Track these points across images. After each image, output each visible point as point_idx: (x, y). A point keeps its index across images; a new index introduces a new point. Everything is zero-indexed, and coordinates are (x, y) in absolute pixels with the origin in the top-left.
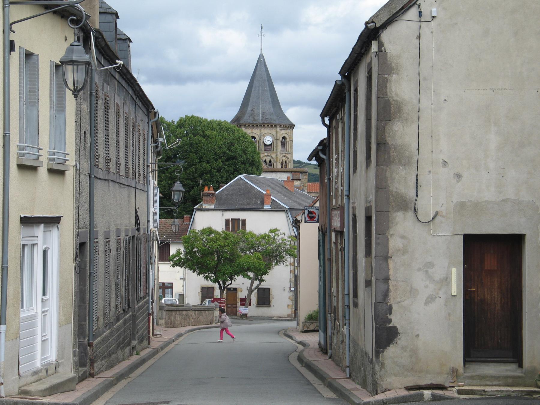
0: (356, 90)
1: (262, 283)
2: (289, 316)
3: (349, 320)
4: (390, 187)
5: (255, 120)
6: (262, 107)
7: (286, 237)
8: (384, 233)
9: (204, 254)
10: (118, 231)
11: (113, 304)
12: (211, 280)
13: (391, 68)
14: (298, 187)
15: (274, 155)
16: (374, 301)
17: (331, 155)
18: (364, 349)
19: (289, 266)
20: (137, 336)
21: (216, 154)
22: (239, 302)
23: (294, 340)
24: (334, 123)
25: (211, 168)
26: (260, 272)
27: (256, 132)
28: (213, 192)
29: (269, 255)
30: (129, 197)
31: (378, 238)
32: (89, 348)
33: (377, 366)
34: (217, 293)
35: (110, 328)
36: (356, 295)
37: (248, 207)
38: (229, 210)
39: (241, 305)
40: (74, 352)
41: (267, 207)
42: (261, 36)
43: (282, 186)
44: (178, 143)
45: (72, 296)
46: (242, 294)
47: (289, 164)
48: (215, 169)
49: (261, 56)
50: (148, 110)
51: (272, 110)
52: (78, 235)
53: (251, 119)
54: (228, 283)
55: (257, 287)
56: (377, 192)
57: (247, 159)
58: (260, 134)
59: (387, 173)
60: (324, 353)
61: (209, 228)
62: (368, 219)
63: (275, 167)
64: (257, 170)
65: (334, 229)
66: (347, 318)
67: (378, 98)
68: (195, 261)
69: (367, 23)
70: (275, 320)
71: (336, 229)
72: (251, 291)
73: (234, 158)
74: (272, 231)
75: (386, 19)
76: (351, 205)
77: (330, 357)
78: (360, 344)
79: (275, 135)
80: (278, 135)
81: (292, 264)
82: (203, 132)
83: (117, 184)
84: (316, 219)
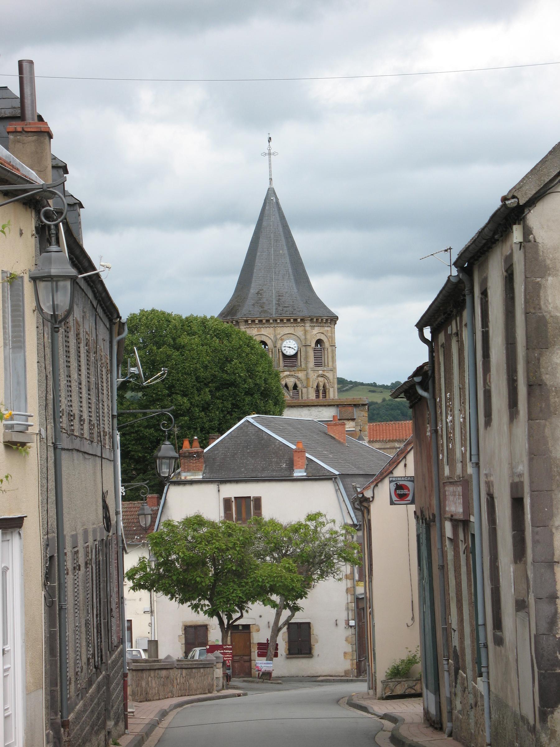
0: (484, 293)
1: (297, 613)
2: (347, 673)
3: (488, 667)
4: (551, 452)
5: (265, 312)
6: (275, 285)
7: (337, 528)
8: (544, 523)
9: (191, 564)
10: (86, 532)
11: (84, 659)
12: (205, 613)
13: (545, 266)
14: (351, 433)
15: (301, 375)
16: (534, 632)
17: (437, 392)
18: (518, 712)
19: (344, 581)
20: (112, 713)
21: (197, 378)
22: (255, 651)
23: (372, 714)
24: (442, 338)
25: (191, 403)
26: (292, 593)
27: (265, 333)
28: (200, 450)
29: (308, 561)
30: (95, 473)
31: (537, 533)
32: (62, 729)
33: (544, 735)
34: (215, 635)
35: (82, 698)
36: (498, 624)
37: (265, 474)
38: (230, 482)
39: (259, 655)
40: (47, 735)
41: (299, 473)
42: (270, 154)
43: (324, 434)
44: (162, 375)
45: (41, 646)
46: (261, 636)
47: (331, 390)
48: (197, 406)
49: (271, 192)
50: (111, 320)
51: (296, 290)
52: (48, 545)
53: (257, 309)
54: (235, 616)
55: (287, 623)
56: (531, 460)
57: (256, 384)
58: (275, 336)
59: (546, 430)
60: (436, 729)
61: (198, 516)
62: (517, 503)
63: (305, 397)
64: (275, 404)
65: (452, 516)
66: (484, 664)
67: (527, 313)
68: (174, 578)
69: (504, 199)
70: (322, 681)
71: (454, 517)
72: (276, 630)
73: (233, 384)
74: (310, 518)
75: (534, 192)
76: (483, 479)
77: (450, 735)
78: (510, 704)
79: (303, 337)
80: (308, 337)
81: (350, 577)
82: (174, 339)
83: (81, 454)
84: (410, 498)
